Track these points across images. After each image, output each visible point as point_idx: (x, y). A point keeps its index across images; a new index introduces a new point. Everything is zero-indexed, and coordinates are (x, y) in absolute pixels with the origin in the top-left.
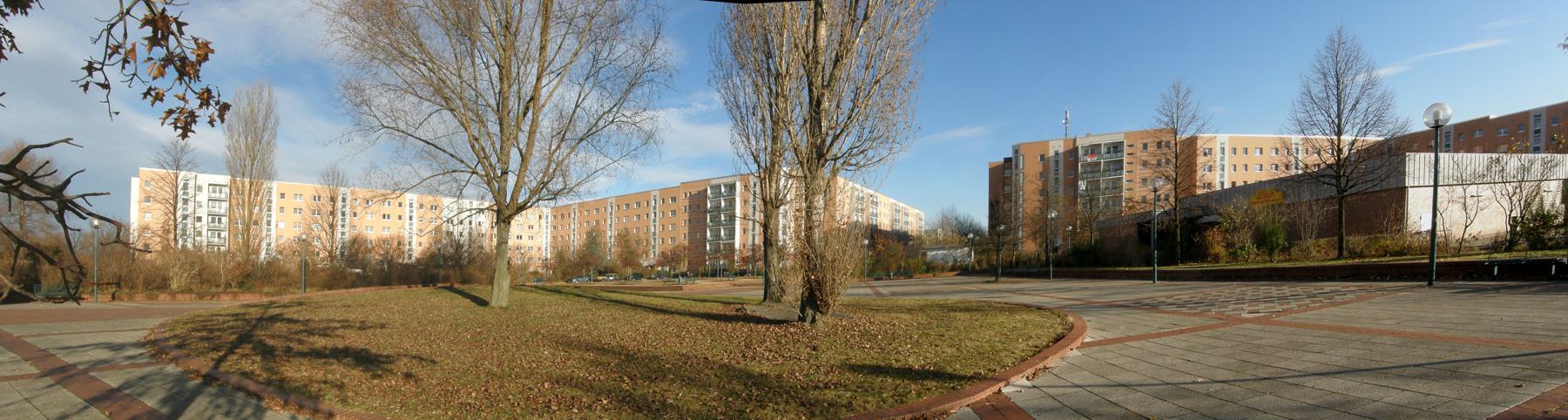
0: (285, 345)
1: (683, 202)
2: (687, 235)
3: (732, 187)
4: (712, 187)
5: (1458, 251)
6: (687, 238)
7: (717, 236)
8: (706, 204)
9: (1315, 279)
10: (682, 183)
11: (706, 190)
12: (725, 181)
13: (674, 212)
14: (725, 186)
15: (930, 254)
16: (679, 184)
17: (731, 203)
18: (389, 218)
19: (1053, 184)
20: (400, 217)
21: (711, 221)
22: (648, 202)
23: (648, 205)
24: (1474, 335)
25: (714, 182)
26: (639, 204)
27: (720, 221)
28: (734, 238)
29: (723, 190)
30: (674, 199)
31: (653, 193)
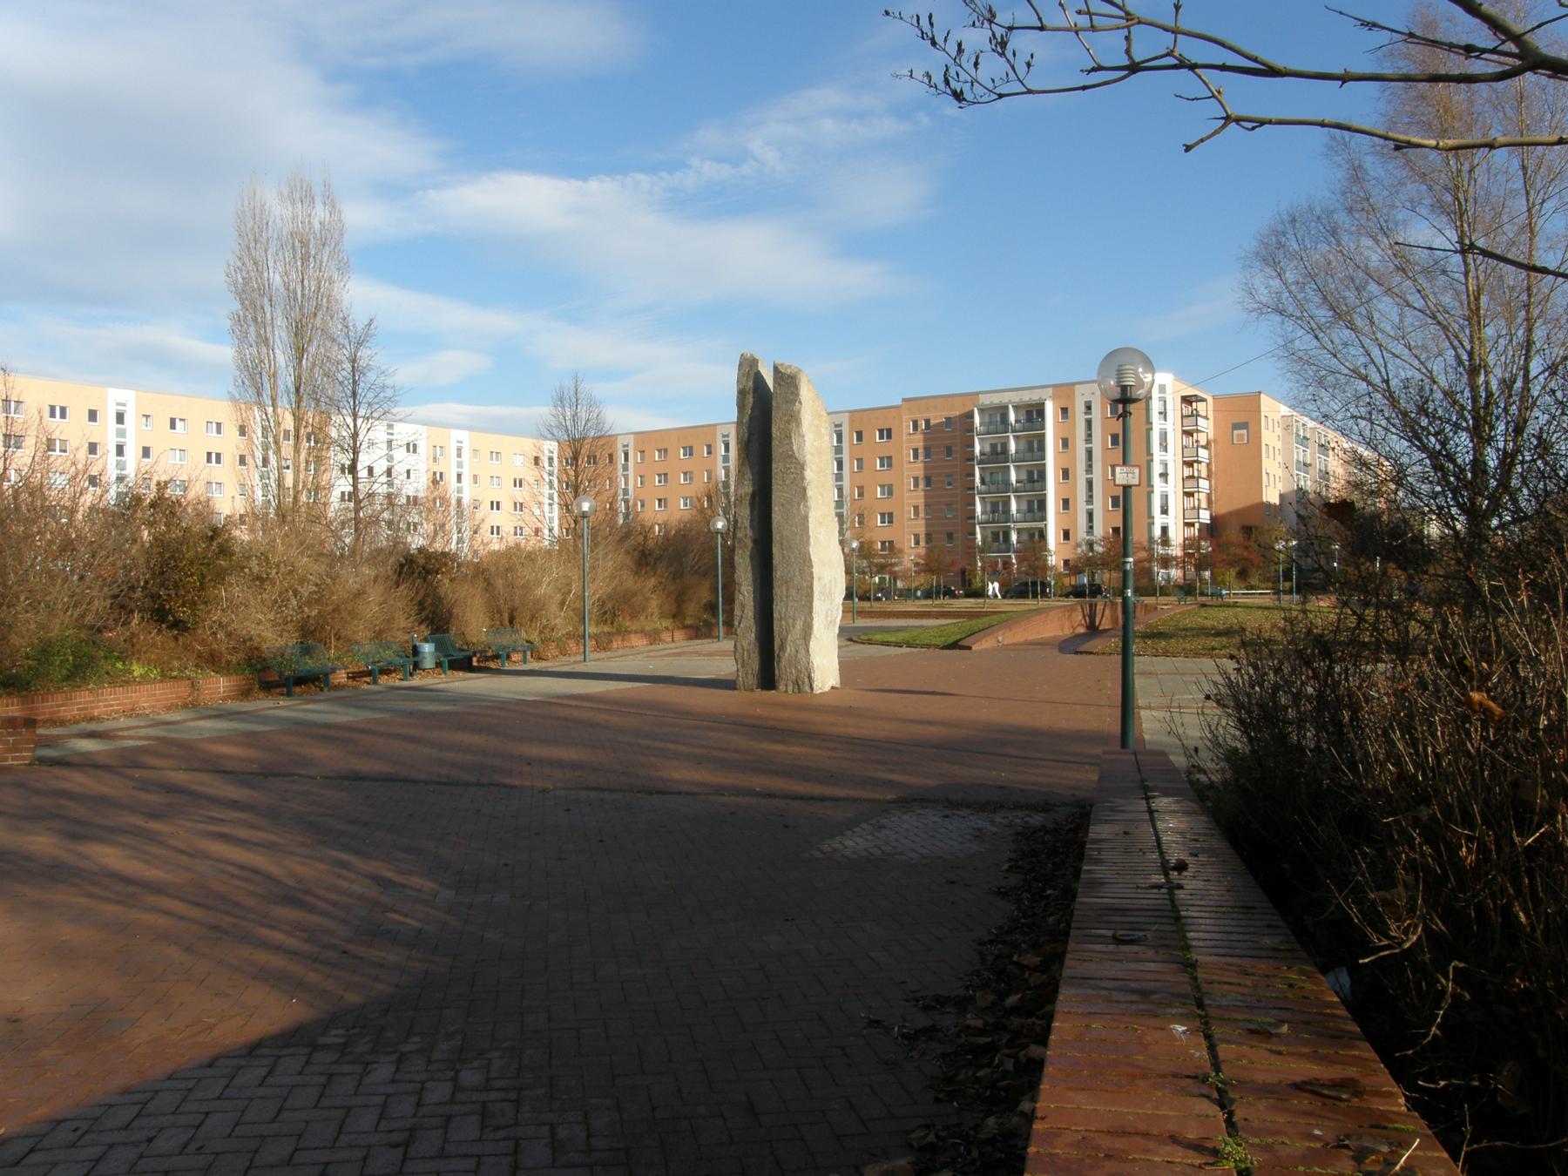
0: (1234, 745)
1: (909, 441)
2: (922, 508)
3: (1034, 413)
4: (982, 411)
5: (778, 656)
6: (922, 515)
7: (998, 509)
8: (973, 446)
9: (531, 670)
10: (904, 400)
11: (970, 415)
12: (1015, 397)
13: (887, 461)
14: (1016, 408)
15: (13, 636)
16: (900, 403)
17: (1035, 447)
18: (63, 416)
19: (739, 552)
20: (93, 416)
21: (983, 482)
22: (709, 447)
23: (709, 453)
24: (567, 712)
25: (986, 400)
26: (689, 451)
27: (1007, 482)
28: (1044, 519)
29: (1012, 417)
30: (887, 433)
31: (720, 431)
